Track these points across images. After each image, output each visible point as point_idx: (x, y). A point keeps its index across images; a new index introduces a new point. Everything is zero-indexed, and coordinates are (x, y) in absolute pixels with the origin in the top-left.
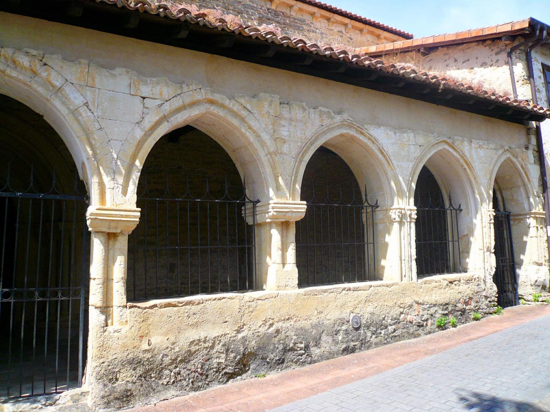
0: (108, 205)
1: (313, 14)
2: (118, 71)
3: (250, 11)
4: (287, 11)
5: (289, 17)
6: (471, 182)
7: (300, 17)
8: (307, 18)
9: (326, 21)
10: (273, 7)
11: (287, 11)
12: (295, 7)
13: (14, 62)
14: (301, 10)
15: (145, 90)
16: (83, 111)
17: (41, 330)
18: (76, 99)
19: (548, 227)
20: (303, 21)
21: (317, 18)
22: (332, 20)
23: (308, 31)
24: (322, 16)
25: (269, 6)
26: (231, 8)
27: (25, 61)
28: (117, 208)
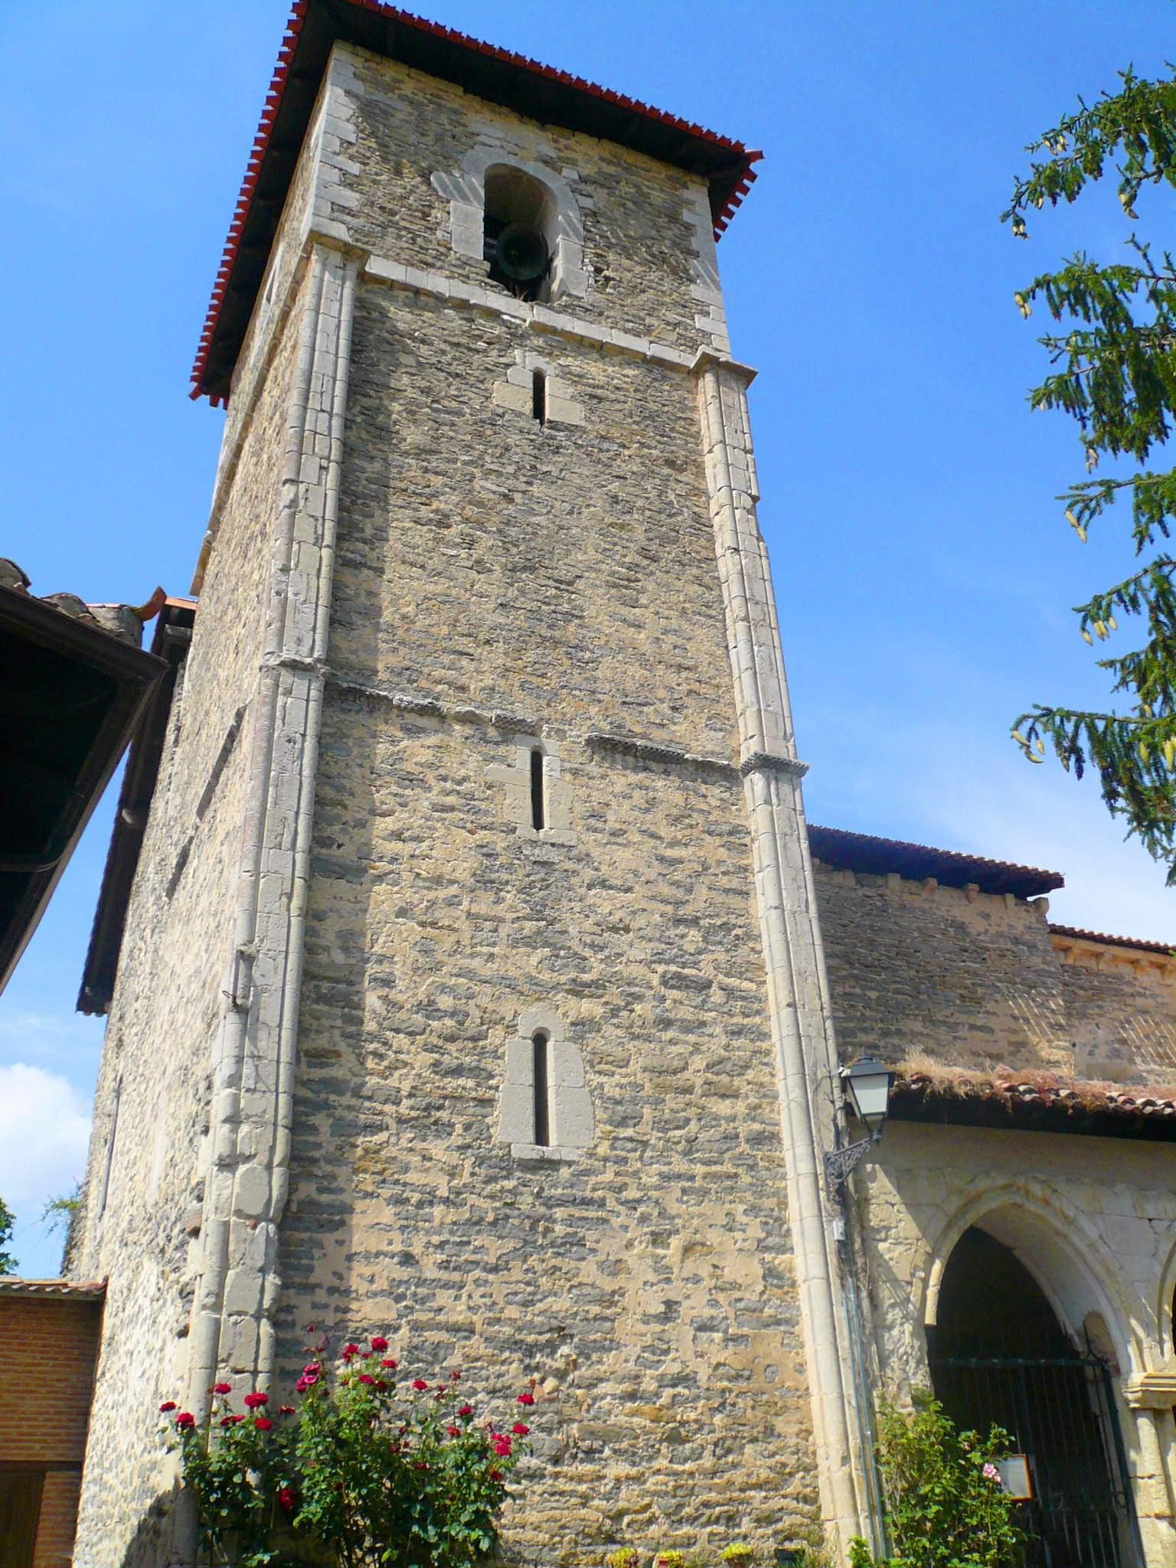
0: (1151, 1371)
1: (1134, 963)
2: (1120, 1187)
3: (1049, 981)
4: (1092, 964)
5: (1097, 975)
6: (1100, 1282)
7: (1115, 970)
8: (1126, 970)
9: (1157, 972)
10: (1070, 961)
11: (1092, 964)
12: (1107, 957)
13: (1027, 1192)
14: (1115, 958)
15: (1151, 1210)
16: (1099, 1244)
17: (1097, 1549)
18: (1092, 1231)
19: (1169, 518)
20: (1119, 977)
21: (1142, 969)
22: (1169, 967)
23: (1133, 995)
24: (1152, 964)
25: (1062, 960)
26: (1018, 980)
27: (1037, 1189)
28: (1162, 1374)
